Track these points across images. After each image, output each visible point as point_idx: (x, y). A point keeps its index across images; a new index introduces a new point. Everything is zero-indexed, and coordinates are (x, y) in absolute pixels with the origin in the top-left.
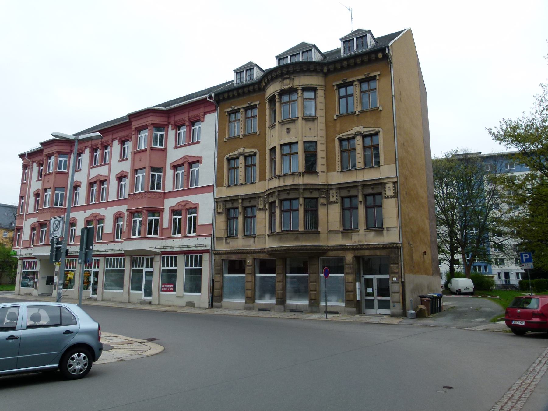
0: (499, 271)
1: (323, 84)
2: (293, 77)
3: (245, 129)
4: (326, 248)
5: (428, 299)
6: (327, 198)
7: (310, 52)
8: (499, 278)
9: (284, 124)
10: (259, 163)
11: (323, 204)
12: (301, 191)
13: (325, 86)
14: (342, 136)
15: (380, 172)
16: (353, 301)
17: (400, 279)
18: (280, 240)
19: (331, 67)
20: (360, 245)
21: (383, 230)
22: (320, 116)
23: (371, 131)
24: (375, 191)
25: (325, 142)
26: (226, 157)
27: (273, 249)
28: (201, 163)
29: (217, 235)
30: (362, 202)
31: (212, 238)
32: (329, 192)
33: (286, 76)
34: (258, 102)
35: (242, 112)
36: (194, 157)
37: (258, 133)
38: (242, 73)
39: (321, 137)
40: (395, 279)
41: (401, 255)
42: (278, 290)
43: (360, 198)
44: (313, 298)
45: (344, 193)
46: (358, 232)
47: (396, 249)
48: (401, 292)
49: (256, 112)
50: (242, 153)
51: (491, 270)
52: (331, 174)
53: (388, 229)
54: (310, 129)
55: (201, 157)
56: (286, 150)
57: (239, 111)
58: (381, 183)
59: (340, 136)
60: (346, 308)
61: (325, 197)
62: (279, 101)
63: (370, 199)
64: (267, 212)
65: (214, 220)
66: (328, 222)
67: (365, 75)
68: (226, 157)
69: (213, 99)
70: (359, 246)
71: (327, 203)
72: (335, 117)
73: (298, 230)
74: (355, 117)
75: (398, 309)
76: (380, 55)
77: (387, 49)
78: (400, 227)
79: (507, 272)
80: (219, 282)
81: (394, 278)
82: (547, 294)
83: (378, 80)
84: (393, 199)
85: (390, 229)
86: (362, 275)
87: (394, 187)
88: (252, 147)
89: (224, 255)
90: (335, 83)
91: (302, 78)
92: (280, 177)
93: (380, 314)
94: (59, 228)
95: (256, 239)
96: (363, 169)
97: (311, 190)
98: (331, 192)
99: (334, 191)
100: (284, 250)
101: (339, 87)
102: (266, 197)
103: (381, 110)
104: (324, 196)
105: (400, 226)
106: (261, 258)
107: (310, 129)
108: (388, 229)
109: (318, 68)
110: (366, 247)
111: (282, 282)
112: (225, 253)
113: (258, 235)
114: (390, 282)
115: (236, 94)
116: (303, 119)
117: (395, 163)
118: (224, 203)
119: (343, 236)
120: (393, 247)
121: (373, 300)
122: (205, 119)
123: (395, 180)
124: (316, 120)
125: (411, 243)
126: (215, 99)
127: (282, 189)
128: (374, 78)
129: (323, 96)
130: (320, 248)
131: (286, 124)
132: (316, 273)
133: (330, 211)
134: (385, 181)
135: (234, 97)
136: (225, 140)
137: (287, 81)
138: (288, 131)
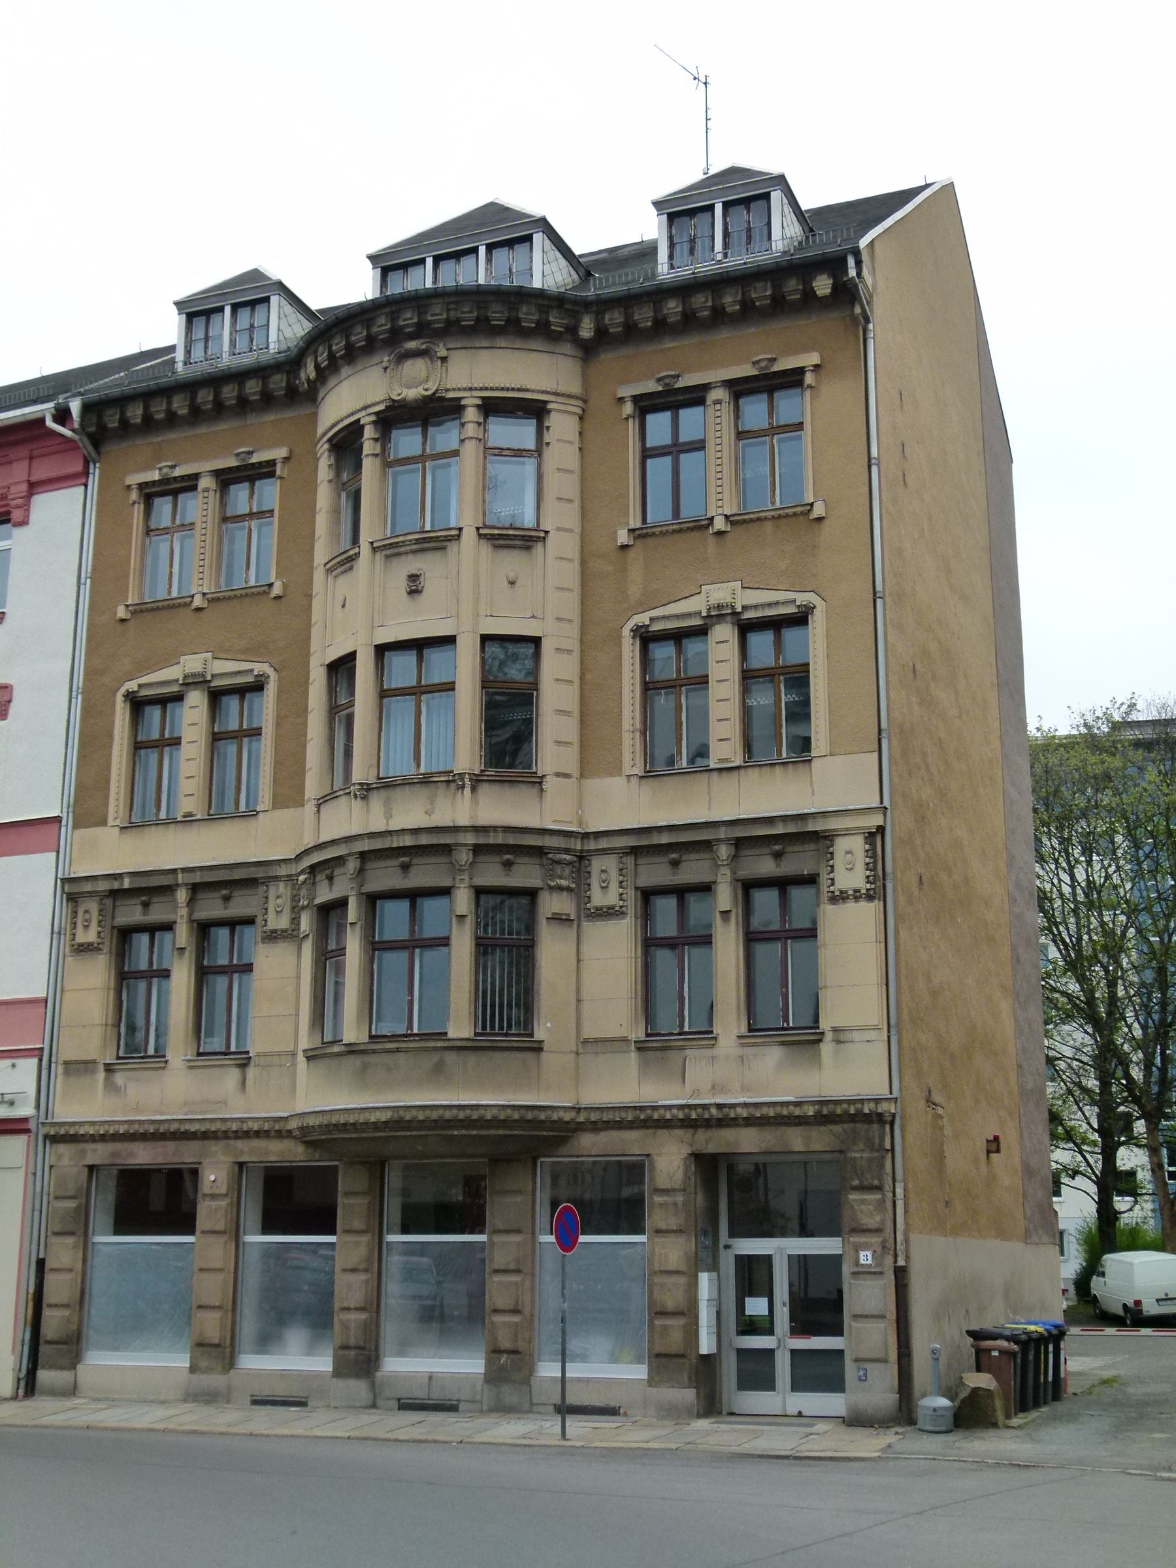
1: (575, 388)
4: (567, 1117)
6: (580, 891)
7: (521, 249)
11: (559, 919)
12: (464, 856)
14: (652, 619)
17: (889, 1260)
18: (362, 1079)
19: (614, 319)
20: (719, 1106)
22: (559, 529)
24: (788, 867)
25: (575, 645)
26: (122, 691)
27: (325, 1120)
29: (69, 1050)
33: (412, 345)
35: (206, 490)
37: (277, 590)
38: (215, 318)
39: (559, 619)
40: (866, 1257)
42: (348, 1309)
43: (724, 897)
44: (506, 1344)
45: (656, 873)
47: (876, 1126)
48: (892, 1315)
49: (270, 493)
52: (594, 784)
54: (512, 583)
56: (403, 669)
58: (816, 836)
59: (643, 619)
66: (579, 1001)
68: (122, 691)
70: (714, 1111)
72: (623, 537)
74: (712, 541)
76: (823, 285)
77: (851, 262)
80: (70, 1270)
81: (862, 1254)
83: (810, 387)
84: (863, 904)
87: (871, 853)
88: (251, 652)
89: (100, 1147)
92: (368, 790)
95: (251, 1072)
98: (597, 864)
99: (610, 863)
100: (377, 1126)
101: (646, 405)
102: (302, 878)
103: (820, 519)
104: (564, 883)
105: (893, 1022)
107: (512, 583)
108: (842, 1037)
109: (556, 320)
111: (366, 1270)
112: (103, 1138)
115: (183, 412)
116: (480, 535)
117: (876, 747)
119: (644, 1065)
123: (876, 820)
124: (540, 545)
125: (937, 1098)
126: (82, 424)
127: (378, 844)
130: (542, 1117)
134: (832, 824)
136: (121, 613)
137: (416, 368)
138: (414, 585)
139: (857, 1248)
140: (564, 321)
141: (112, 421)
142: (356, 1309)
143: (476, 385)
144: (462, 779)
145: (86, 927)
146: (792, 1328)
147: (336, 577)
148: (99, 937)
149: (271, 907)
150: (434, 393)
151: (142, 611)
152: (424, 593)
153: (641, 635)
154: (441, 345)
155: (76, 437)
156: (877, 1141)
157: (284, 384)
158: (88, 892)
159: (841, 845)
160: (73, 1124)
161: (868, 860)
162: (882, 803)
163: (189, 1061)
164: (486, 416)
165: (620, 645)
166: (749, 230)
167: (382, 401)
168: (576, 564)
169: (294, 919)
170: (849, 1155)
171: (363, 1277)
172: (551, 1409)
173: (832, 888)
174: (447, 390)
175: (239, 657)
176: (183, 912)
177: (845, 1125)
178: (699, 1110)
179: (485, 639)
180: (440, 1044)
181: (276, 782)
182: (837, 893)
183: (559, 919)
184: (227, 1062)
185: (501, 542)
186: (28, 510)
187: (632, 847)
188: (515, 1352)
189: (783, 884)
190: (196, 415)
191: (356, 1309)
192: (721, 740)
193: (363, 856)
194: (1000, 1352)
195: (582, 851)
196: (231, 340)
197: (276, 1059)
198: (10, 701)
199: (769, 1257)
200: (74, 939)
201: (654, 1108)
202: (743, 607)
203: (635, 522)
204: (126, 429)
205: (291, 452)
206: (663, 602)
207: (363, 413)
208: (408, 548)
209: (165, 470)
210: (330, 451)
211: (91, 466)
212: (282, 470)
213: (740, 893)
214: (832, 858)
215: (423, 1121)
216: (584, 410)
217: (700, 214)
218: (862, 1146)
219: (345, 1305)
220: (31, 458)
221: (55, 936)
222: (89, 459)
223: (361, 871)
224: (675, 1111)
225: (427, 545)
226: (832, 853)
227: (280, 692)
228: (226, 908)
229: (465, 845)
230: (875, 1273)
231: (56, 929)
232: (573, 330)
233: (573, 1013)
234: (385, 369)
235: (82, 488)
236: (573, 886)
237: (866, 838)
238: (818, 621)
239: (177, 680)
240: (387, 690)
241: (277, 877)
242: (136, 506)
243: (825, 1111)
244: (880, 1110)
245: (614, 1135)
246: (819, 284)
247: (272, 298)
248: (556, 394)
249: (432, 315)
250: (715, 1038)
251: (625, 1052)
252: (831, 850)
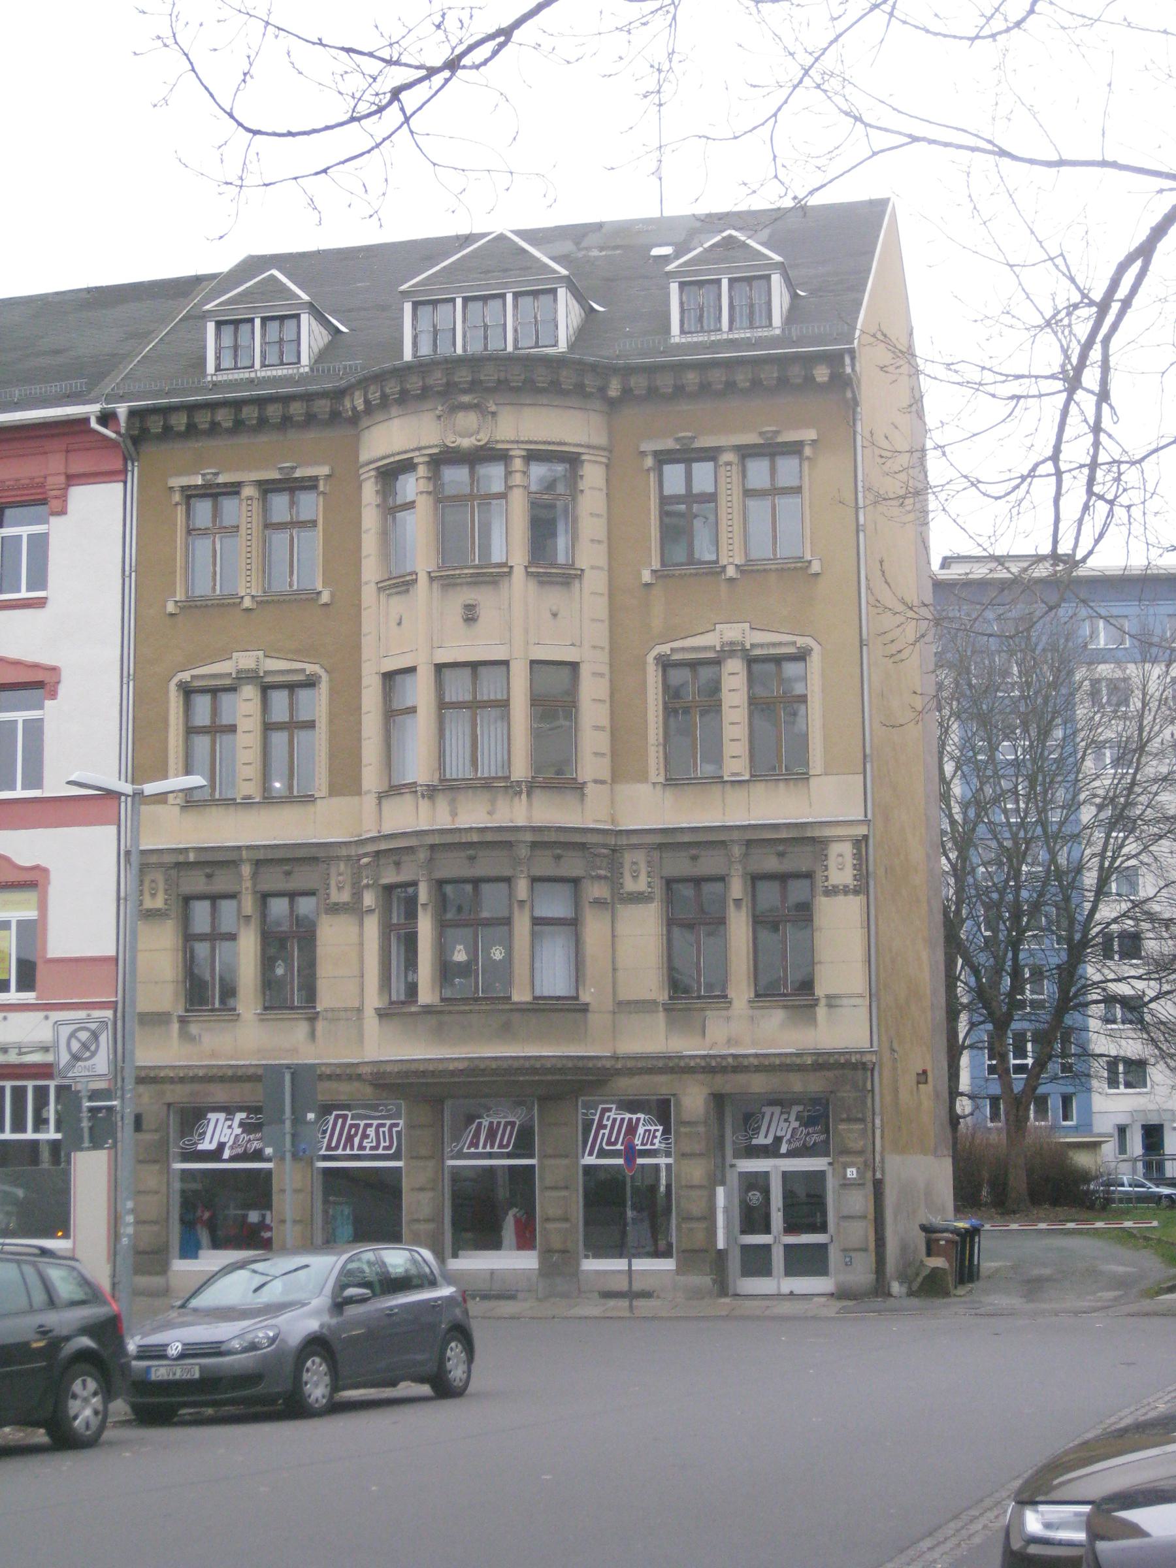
0: (1122, 1120)
1: (601, 440)
2: (493, 408)
3: (264, 572)
4: (608, 1064)
5: (950, 1235)
6: (614, 880)
7: (545, 299)
8: (1122, 1148)
9: (455, 585)
10: (331, 722)
11: (599, 903)
12: (523, 852)
13: (609, 449)
14: (672, 649)
15: (809, 792)
16: (706, 1251)
17: (869, 1174)
18: (439, 1034)
19: (639, 383)
20: (735, 1056)
21: (814, 1005)
22: (593, 568)
23: (780, 644)
24: (787, 866)
25: (605, 669)
26: (175, 680)
27: (404, 1067)
28: (53, 695)
29: (144, 1004)
30: (744, 903)
31: (119, 1014)
32: (622, 857)
33: (466, 399)
34: (324, 470)
35: (250, 498)
36: (17, 663)
37: (325, 598)
38: (244, 328)
39: (594, 647)
40: (852, 1173)
41: (873, 1091)
42: (418, 1221)
43: (737, 888)
44: (557, 1245)
45: (679, 866)
46: (727, 1009)
47: (860, 1072)
48: (871, 1216)
49: (310, 505)
50: (256, 671)
51: (1087, 1111)
52: (626, 790)
53: (832, 1001)
54: (555, 615)
55: (54, 670)
56: (459, 688)
57: (237, 493)
58: (813, 840)
59: (665, 649)
60: (682, 1278)
61: (606, 878)
62: (431, 489)
63: (769, 894)
64: (372, 926)
65: (127, 937)
66: (614, 970)
67: (761, 434)
68: (175, 680)
69: (123, 431)
70: (730, 1060)
71: (613, 898)
72: (646, 576)
73: (510, 998)
74: (724, 587)
75: (861, 1274)
76: (822, 374)
77: (847, 360)
78: (873, 995)
79: (1154, 1120)
80: (157, 1193)
81: (849, 1171)
82: (5, 1050)
83: (808, 458)
84: (851, 897)
85: (838, 1002)
86: (729, 1159)
87: (858, 856)
88: (299, 653)
89: (178, 1088)
90: (649, 446)
91: (528, 412)
92: (434, 790)
93: (791, 1293)
94: (93, 1054)
95: (320, 1026)
96: (747, 781)
97: (559, 851)
98: (628, 858)
99: (640, 857)
100: (453, 1073)
101: (663, 458)
102: (365, 860)
103: (817, 575)
104: (602, 872)
105: (873, 991)
106: (343, 1097)
107: (555, 615)
108: (833, 1002)
109: (590, 382)
110: (755, 1062)
111: (433, 1189)
112: (182, 1080)
113: (326, 1010)
114: (831, 1183)
115: (228, 424)
116: (527, 573)
117: (861, 770)
118: (173, 872)
119: (671, 1024)
120: (848, 1065)
121: (767, 1248)
122: (71, 506)
123: (862, 830)
124: (577, 582)
125: (896, 1046)
126: (128, 428)
127: (449, 839)
128: (795, 448)
129: (601, 490)
130: (590, 1065)
131: (461, 584)
132: (567, 1156)
133: (621, 929)
134: (828, 832)
135: (214, 429)
136: (171, 607)
137: (467, 420)
138: (470, 615)
139: (845, 1166)
140: (597, 384)
141: (155, 425)
142: (424, 1221)
143: (522, 439)
144: (520, 786)
145: (153, 895)
146: (784, 1228)
147: (389, 595)
148: (166, 904)
149: (333, 883)
150: (486, 444)
151: (190, 607)
152: (481, 620)
153: (662, 663)
154: (491, 402)
155: (120, 439)
156: (860, 1083)
157: (328, 409)
158: (153, 864)
159: (835, 849)
160: (150, 1068)
161: (855, 862)
162: (866, 816)
163: (259, 1014)
164: (528, 465)
165: (644, 671)
166: (751, 306)
167: (436, 446)
168: (606, 598)
169: (354, 894)
170: (839, 1094)
171: (430, 1194)
172: (596, 1294)
173: (826, 884)
174: (497, 442)
175: (290, 656)
176: (247, 884)
177: (836, 1072)
178: (719, 1060)
179: (533, 663)
180: (508, 1007)
181: (331, 770)
182: (830, 888)
183: (599, 903)
184: (297, 1016)
185: (544, 579)
186: (65, 501)
187: (660, 844)
188: (564, 1252)
189: (783, 878)
190: (239, 426)
191: (424, 1221)
192: (734, 757)
193: (433, 847)
194: (947, 1241)
195: (615, 845)
196: (261, 352)
197: (343, 1014)
198: (58, 683)
199: (767, 1173)
200: (141, 904)
201: (682, 1057)
202: (752, 645)
203: (656, 565)
204: (168, 433)
205: (332, 469)
206: (682, 636)
207: (417, 453)
208: (464, 580)
209: (209, 477)
210: (376, 477)
211: (129, 464)
212: (325, 485)
213: (749, 883)
214: (826, 859)
215: (496, 1069)
216: (609, 459)
217: (707, 285)
218: (848, 1087)
219: (415, 1217)
220: (67, 451)
221: (122, 901)
222: (127, 456)
223: (431, 860)
224: (698, 1060)
225: (481, 579)
226: (826, 855)
227: (333, 691)
228: (287, 882)
229: (525, 842)
230: (859, 1185)
231: (122, 894)
232: (603, 390)
233: (610, 980)
234: (439, 417)
235: (121, 485)
236: (609, 875)
237: (854, 844)
238: (815, 660)
239: (231, 674)
240: (447, 703)
241: (337, 856)
242: (179, 507)
243: (820, 1061)
244: (864, 1060)
245: (646, 1078)
246: (820, 372)
247: (302, 316)
248: (588, 447)
249: (485, 375)
250: (730, 1003)
251: (653, 1012)
252: (825, 852)
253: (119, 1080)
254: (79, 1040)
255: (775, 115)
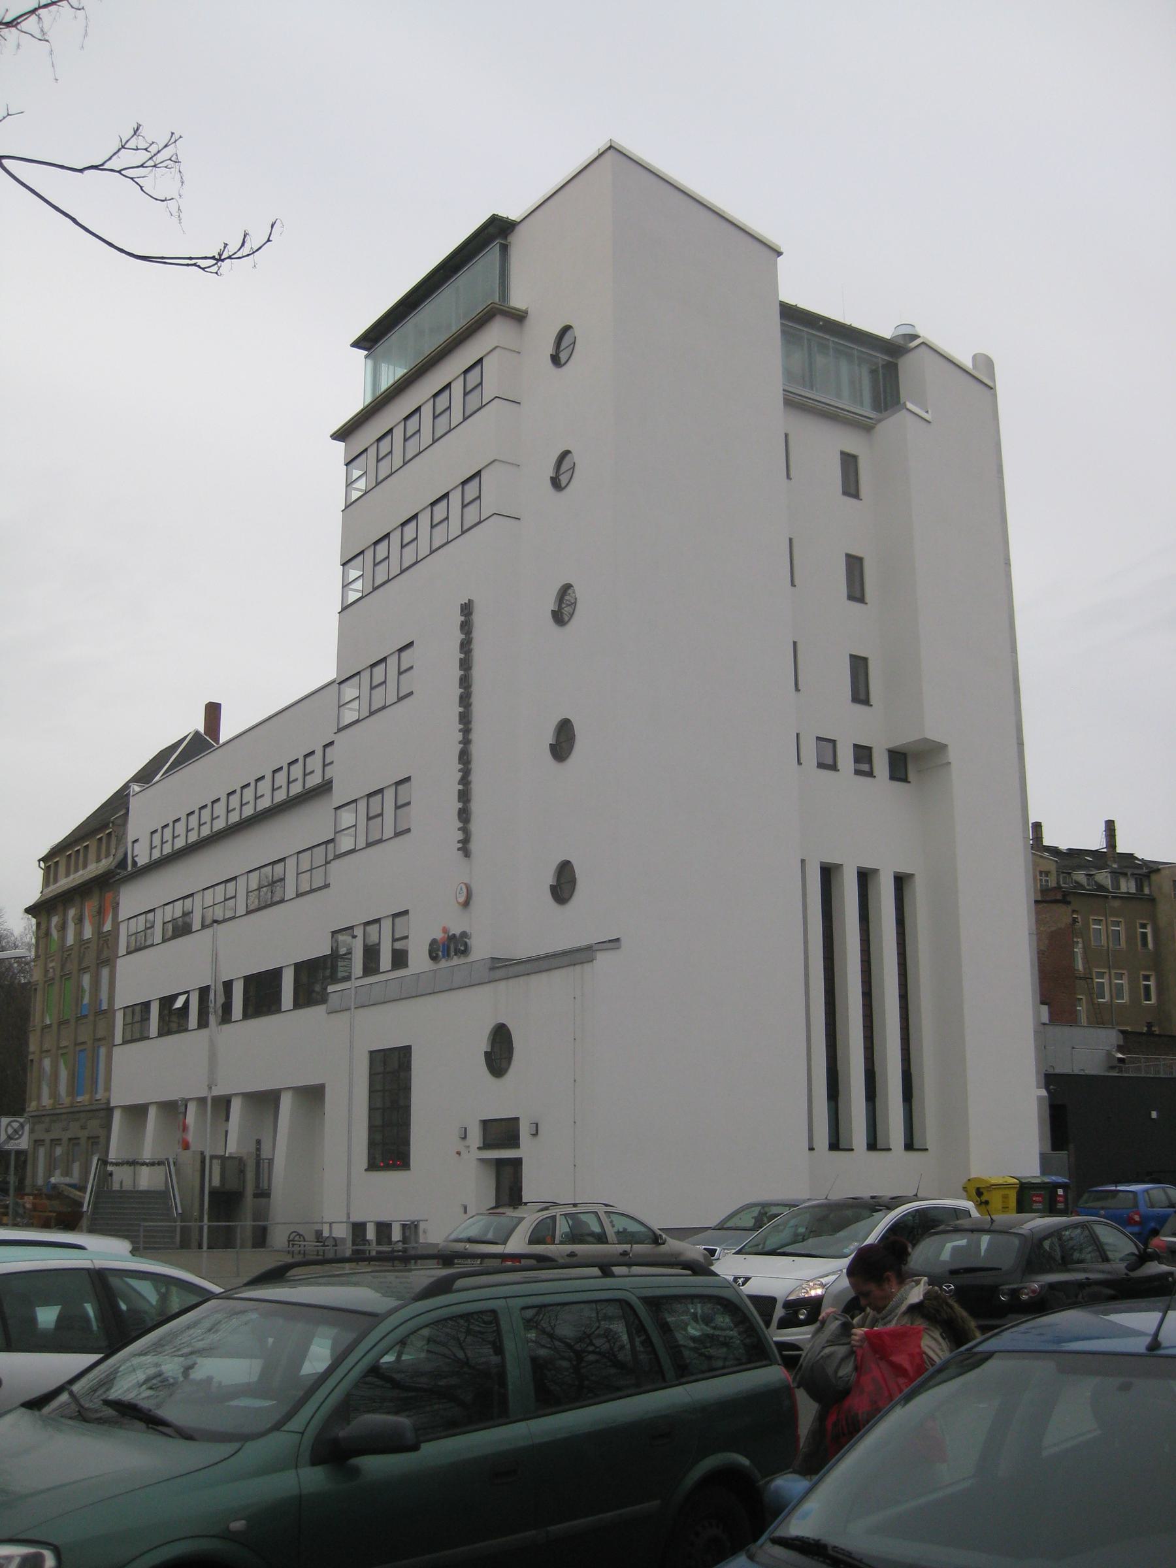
94: (20, 1136)
253: (62, 1003)
254: (13, 1127)
255: (119, 172)
